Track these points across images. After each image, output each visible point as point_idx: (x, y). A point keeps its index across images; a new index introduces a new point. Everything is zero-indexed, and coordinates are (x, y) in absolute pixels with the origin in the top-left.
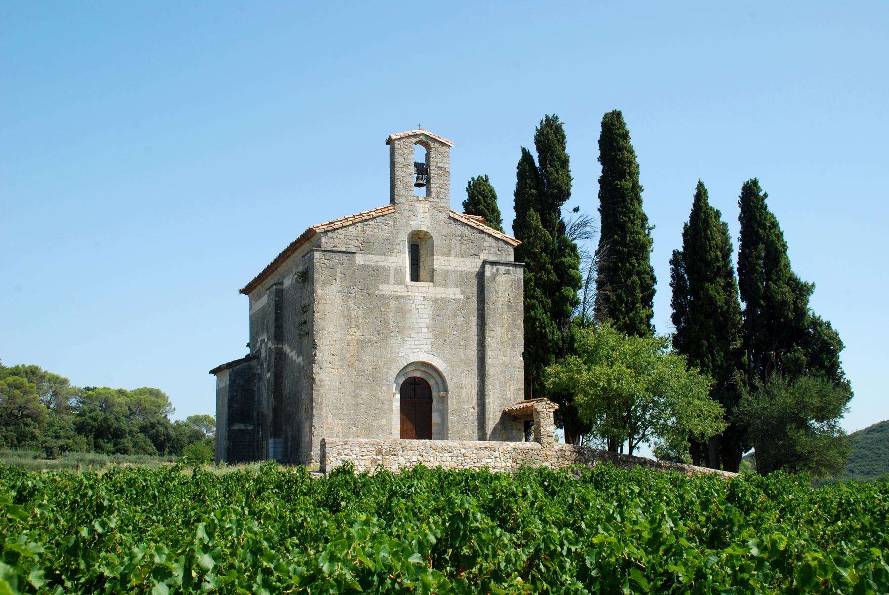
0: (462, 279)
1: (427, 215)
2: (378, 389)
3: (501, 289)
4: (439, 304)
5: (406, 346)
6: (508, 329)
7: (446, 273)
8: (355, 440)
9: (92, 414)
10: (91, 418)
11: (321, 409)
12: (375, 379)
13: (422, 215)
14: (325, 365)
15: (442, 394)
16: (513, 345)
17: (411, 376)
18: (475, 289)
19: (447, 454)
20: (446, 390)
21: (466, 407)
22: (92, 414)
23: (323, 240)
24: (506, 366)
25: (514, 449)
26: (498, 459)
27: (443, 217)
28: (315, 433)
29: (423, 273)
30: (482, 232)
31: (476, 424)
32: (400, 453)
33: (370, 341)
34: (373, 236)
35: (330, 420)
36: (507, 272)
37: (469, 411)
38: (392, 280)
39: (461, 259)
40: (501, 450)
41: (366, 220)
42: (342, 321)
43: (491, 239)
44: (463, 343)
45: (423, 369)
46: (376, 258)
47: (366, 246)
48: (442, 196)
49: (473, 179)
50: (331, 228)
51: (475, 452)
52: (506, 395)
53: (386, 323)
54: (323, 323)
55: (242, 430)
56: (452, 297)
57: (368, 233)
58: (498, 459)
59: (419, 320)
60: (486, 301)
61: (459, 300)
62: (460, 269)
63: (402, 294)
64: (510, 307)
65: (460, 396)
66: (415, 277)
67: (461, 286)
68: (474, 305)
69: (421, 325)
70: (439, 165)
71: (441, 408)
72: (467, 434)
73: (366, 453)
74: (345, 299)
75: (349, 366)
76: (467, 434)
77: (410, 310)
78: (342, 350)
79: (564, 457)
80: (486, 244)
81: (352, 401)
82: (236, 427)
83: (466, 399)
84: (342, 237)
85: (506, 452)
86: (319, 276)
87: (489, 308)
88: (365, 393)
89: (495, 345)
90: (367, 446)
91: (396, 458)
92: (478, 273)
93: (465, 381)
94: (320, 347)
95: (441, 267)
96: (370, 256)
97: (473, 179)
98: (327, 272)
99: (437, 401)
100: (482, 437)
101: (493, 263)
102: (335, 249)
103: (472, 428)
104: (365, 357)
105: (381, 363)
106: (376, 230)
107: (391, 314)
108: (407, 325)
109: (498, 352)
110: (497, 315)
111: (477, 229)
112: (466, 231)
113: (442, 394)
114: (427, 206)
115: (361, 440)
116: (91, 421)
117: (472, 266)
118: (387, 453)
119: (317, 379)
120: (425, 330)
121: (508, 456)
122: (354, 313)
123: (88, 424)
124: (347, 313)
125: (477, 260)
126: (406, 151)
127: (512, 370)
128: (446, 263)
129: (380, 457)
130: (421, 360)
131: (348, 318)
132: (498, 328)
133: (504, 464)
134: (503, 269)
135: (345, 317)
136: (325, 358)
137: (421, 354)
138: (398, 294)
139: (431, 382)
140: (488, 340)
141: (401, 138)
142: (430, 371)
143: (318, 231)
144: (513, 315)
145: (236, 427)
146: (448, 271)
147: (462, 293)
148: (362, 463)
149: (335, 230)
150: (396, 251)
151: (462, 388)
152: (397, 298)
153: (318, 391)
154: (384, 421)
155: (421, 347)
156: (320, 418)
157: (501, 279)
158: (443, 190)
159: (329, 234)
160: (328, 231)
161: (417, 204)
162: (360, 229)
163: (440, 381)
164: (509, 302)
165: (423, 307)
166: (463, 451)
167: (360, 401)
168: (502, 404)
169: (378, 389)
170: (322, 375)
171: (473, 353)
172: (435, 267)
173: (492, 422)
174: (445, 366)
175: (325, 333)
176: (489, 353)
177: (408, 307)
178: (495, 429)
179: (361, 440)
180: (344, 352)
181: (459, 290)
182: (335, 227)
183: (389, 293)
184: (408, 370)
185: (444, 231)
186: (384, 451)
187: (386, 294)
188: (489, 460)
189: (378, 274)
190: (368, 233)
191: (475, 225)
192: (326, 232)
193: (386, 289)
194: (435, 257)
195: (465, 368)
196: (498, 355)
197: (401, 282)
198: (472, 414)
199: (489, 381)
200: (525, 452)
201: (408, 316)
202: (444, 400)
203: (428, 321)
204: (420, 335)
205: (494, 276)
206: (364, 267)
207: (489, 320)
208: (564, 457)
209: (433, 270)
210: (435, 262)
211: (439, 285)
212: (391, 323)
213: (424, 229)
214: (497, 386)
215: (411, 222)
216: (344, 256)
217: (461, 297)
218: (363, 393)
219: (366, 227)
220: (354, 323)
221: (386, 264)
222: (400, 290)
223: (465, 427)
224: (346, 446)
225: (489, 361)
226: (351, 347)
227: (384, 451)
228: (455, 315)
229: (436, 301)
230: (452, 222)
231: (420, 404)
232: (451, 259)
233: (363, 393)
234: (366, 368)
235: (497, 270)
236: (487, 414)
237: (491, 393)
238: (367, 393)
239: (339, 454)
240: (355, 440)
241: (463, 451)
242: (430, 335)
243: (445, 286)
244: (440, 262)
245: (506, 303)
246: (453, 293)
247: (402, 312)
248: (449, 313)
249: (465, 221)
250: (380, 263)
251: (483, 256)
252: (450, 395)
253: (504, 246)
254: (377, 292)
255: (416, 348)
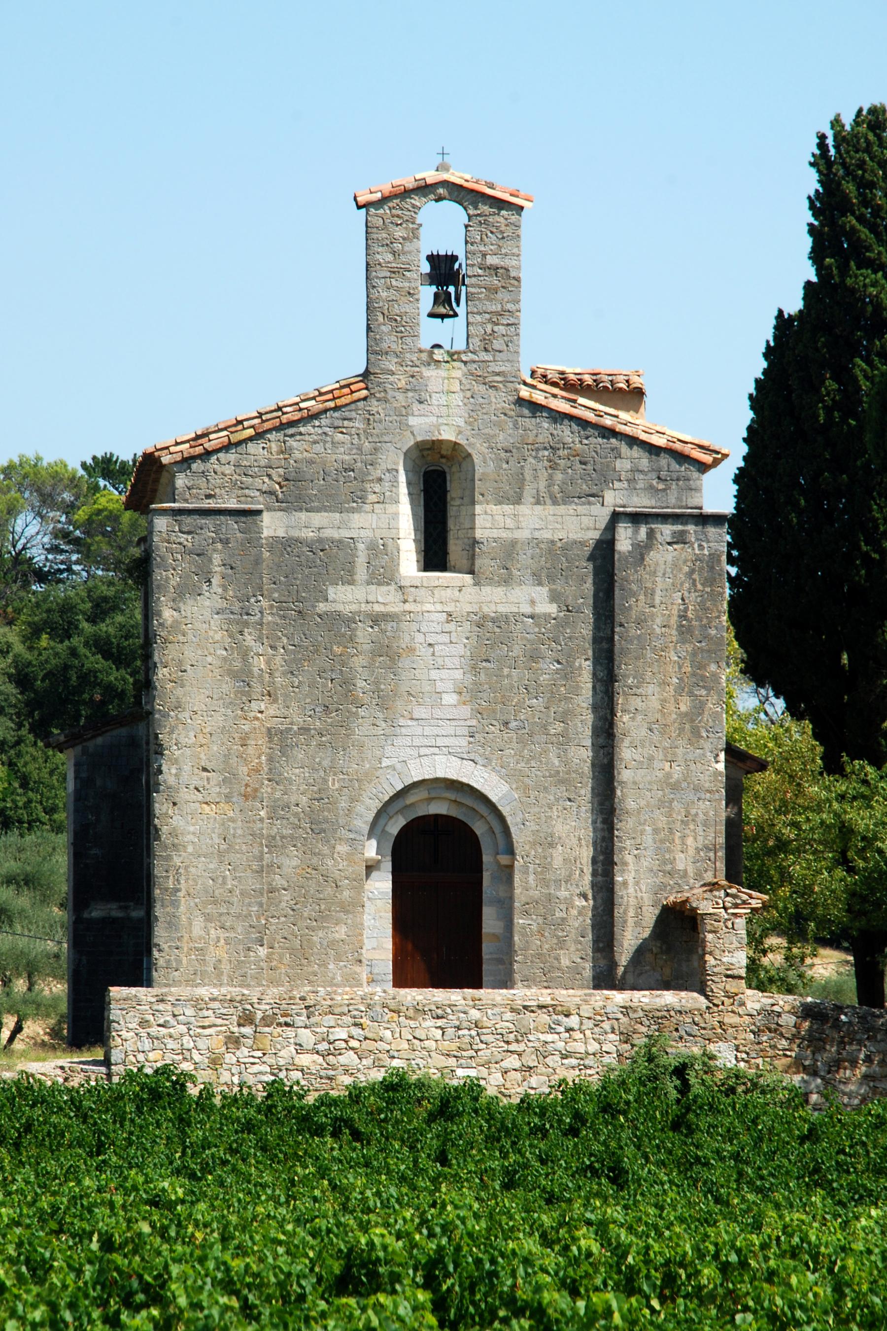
0: (551, 562)
1: (457, 399)
2: (326, 850)
3: (661, 583)
4: (491, 630)
5: (398, 741)
6: (679, 690)
7: (510, 549)
8: (185, 992)
9: (106, 628)
10: (102, 646)
11: (175, 904)
12: (319, 825)
13: (443, 400)
14: (184, 795)
15: (504, 859)
16: (696, 732)
17: (421, 813)
18: (589, 586)
19: (430, 1023)
20: (510, 851)
21: (563, 893)
22: (106, 628)
23: (181, 481)
24: (675, 787)
25: (626, 1010)
26: (578, 1035)
27: (500, 400)
28: (161, 962)
29: (455, 550)
30: (609, 433)
31: (590, 936)
32: (301, 1020)
33: (304, 730)
34: (311, 462)
35: (198, 927)
36: (680, 539)
37: (570, 904)
38: (361, 573)
39: (551, 509)
40: (586, 1011)
41: (292, 424)
42: (228, 686)
43: (636, 452)
44: (557, 728)
45: (452, 795)
46: (318, 519)
47: (293, 492)
48: (497, 344)
49: (836, 123)
50: (199, 450)
51: (508, 1016)
52: (673, 861)
53: (347, 683)
54: (179, 692)
55: (114, 920)
56: (527, 609)
57: (297, 455)
58: (578, 1035)
59: (434, 674)
60: (619, 618)
61: (547, 617)
62: (546, 535)
63: (390, 609)
64: (685, 632)
65: (546, 867)
66: (434, 556)
67: (551, 579)
68: (585, 629)
69: (440, 686)
70: (491, 260)
71: (502, 894)
72: (565, 962)
73: (213, 1020)
74: (234, 629)
75: (246, 796)
76: (565, 962)
77: (411, 650)
78: (227, 756)
79: (776, 1030)
80: (623, 465)
81: (252, 883)
82: (96, 912)
83: (563, 873)
84: (228, 470)
85: (599, 1017)
86: (168, 576)
87: (626, 635)
88: (291, 861)
89: (644, 732)
90: (216, 1005)
91: (290, 1032)
92: (599, 543)
93: (560, 828)
94: (172, 751)
95: (495, 534)
96: (303, 516)
97: (836, 123)
98: (185, 565)
99: (493, 878)
100: (605, 978)
101: (637, 518)
102: (211, 504)
103: (577, 954)
104: (292, 773)
105: (333, 784)
106: (319, 448)
107: (358, 662)
108: (404, 688)
109: (650, 751)
110: (649, 654)
111: (596, 426)
112: (567, 433)
113: (504, 859)
114: (458, 374)
115: (204, 992)
116: (95, 661)
117: (581, 524)
118: (267, 1021)
119: (165, 829)
120: (450, 699)
121: (606, 1026)
122: (260, 663)
123: (88, 678)
124: (238, 664)
125: (596, 509)
126: (399, 233)
127: (692, 797)
128: (510, 523)
129: (247, 1030)
130: (440, 774)
131: (242, 676)
132: (651, 689)
133: (593, 1047)
134: (666, 530)
135: (235, 675)
136: (185, 777)
137: (440, 759)
138: (378, 608)
139: (479, 829)
140: (623, 720)
141: (384, 200)
142: (469, 801)
143: (166, 459)
144: (694, 654)
145: (96, 912)
146: (514, 543)
147: (554, 597)
148: (202, 1044)
149: (208, 454)
150: (372, 498)
151: (551, 845)
152: (376, 619)
153: (169, 858)
154: (341, 932)
155: (440, 742)
156: (172, 925)
157: (663, 556)
158: (501, 329)
159: (196, 466)
160: (193, 458)
161: (428, 372)
162: (274, 447)
163: (498, 829)
164: (683, 616)
165: (445, 638)
166: (475, 1014)
167: (279, 881)
168: (663, 887)
169: (326, 850)
170: (177, 821)
171: (582, 754)
172: (479, 534)
173: (632, 934)
174: (505, 788)
175: (185, 715)
176: (627, 753)
177: (405, 641)
178: (640, 952)
179: (204, 992)
180: (234, 761)
181: (544, 591)
182: (209, 446)
183: (354, 607)
184: (411, 799)
185: (502, 439)
186: (259, 1015)
187: (346, 609)
188: (549, 1037)
189: (326, 561)
190: (297, 455)
191: (590, 416)
192: (186, 461)
193: (344, 598)
194: (478, 509)
195: (561, 791)
196: (651, 759)
197: (384, 573)
198: (579, 910)
199: (625, 827)
200: (659, 1018)
201: (404, 663)
202: (507, 873)
203: (458, 675)
204: (438, 713)
205: (641, 551)
206: (286, 545)
207: (625, 669)
208: (776, 1030)
209: (475, 542)
210: (479, 521)
211: (491, 582)
212: (360, 684)
213: (448, 435)
214: (648, 840)
215: (412, 421)
216: (231, 522)
217: (552, 609)
218: (286, 862)
219: (291, 442)
220: (258, 688)
221: (345, 533)
222: (385, 599)
223: (561, 943)
224: (161, 1007)
225: (625, 775)
226: (251, 750)
227: (259, 1015)
228: (534, 657)
229: (481, 622)
230: (526, 412)
231: (445, 890)
232: (524, 509)
233: (286, 862)
234: (293, 799)
235: (651, 534)
236: (618, 912)
237: (629, 859)
238: (295, 862)
239: (144, 1023)
240: (185, 992)
241: (475, 1014)
242: (466, 711)
243: (507, 581)
244: (490, 520)
245: (674, 620)
246: (529, 599)
247: (388, 654)
248: (517, 651)
249: (563, 406)
250: (328, 533)
251: (614, 498)
252: (519, 863)
253: (675, 466)
254: (322, 607)
255: (429, 743)
